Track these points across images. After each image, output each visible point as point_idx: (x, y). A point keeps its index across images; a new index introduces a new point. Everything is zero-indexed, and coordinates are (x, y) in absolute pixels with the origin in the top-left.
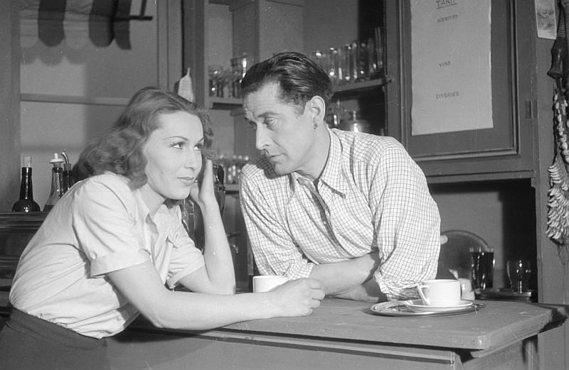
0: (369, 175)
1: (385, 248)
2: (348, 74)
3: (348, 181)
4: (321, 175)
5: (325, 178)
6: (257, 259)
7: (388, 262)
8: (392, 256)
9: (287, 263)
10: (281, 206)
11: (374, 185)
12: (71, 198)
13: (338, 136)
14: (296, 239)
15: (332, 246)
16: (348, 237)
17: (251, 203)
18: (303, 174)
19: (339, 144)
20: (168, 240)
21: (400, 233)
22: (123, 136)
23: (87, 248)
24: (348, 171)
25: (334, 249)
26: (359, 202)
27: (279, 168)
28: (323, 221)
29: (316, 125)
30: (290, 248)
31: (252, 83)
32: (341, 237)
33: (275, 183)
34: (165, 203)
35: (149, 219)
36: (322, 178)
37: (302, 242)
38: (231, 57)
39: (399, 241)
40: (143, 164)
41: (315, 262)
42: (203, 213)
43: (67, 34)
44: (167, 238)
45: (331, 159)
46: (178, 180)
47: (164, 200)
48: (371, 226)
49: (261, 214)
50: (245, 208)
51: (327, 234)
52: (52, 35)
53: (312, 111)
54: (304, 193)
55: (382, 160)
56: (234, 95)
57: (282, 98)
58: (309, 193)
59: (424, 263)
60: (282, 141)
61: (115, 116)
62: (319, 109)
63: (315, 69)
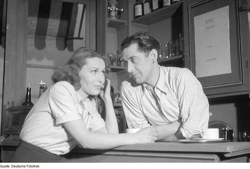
0: (177, 84)
1: (185, 116)
2: (167, 55)
3: (168, 88)
4: (156, 84)
5: (158, 86)
6: (128, 124)
7: (186, 123)
8: (188, 120)
9: (141, 125)
10: (139, 99)
11: (179, 89)
12: (48, 91)
13: (163, 68)
14: (145, 114)
15: (161, 117)
16: (168, 112)
17: (126, 98)
18: (148, 84)
19: (164, 72)
20: (89, 114)
21: (191, 109)
22: (70, 67)
23: (54, 112)
24: (168, 83)
25: (162, 118)
26: (173, 96)
27: (138, 81)
28: (157, 105)
29: (154, 62)
30: (143, 118)
31: (126, 44)
32: (165, 113)
33: (136, 89)
34: (88, 97)
35: (81, 103)
36: (157, 86)
37: (148, 115)
38: (117, 50)
39: (190, 113)
40: (79, 80)
41: (154, 125)
42: (105, 103)
43: (47, 45)
44: (89, 112)
45: (160, 79)
46: (94, 87)
47: (88, 96)
48: (178, 107)
49: (130, 103)
50: (123, 100)
51: (159, 111)
52: (40, 45)
53: (152, 56)
54: (148, 93)
55: (182, 77)
56: (118, 65)
57: (139, 50)
58: (150, 93)
59: (202, 123)
60: (139, 68)
61: (67, 60)
62: (155, 55)
63: (153, 38)
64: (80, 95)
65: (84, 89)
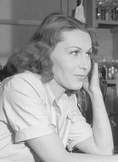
20: (68, 118)
22: (37, 46)
23: (12, 123)
34: (66, 92)
35: (55, 104)
40: (51, 65)
42: (92, 99)
44: (67, 117)
46: (75, 77)
47: (65, 90)
61: (32, 32)
64: (51, 90)
65: (58, 79)
